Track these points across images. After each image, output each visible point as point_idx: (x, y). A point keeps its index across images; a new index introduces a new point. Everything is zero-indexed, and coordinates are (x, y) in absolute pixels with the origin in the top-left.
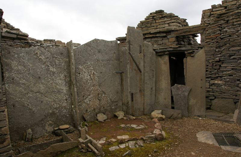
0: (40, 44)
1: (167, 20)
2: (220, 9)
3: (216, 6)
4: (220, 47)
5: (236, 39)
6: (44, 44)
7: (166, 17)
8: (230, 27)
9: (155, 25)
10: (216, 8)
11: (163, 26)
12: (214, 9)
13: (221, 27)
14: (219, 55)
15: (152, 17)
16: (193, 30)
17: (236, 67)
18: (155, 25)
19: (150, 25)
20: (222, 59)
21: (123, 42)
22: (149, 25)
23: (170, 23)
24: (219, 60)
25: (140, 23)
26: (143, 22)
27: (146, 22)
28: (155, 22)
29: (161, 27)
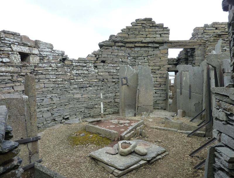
1: (159, 30)
3: (209, 25)
6: (6, 39)
7: (158, 27)
9: (144, 33)
10: (209, 27)
11: (154, 36)
12: (206, 28)
15: (141, 24)
16: (189, 45)
18: (144, 33)
19: (138, 33)
21: (107, 49)
22: (137, 32)
23: (162, 34)
25: (125, 28)
26: (130, 27)
27: (134, 28)
28: (144, 30)
29: (151, 37)
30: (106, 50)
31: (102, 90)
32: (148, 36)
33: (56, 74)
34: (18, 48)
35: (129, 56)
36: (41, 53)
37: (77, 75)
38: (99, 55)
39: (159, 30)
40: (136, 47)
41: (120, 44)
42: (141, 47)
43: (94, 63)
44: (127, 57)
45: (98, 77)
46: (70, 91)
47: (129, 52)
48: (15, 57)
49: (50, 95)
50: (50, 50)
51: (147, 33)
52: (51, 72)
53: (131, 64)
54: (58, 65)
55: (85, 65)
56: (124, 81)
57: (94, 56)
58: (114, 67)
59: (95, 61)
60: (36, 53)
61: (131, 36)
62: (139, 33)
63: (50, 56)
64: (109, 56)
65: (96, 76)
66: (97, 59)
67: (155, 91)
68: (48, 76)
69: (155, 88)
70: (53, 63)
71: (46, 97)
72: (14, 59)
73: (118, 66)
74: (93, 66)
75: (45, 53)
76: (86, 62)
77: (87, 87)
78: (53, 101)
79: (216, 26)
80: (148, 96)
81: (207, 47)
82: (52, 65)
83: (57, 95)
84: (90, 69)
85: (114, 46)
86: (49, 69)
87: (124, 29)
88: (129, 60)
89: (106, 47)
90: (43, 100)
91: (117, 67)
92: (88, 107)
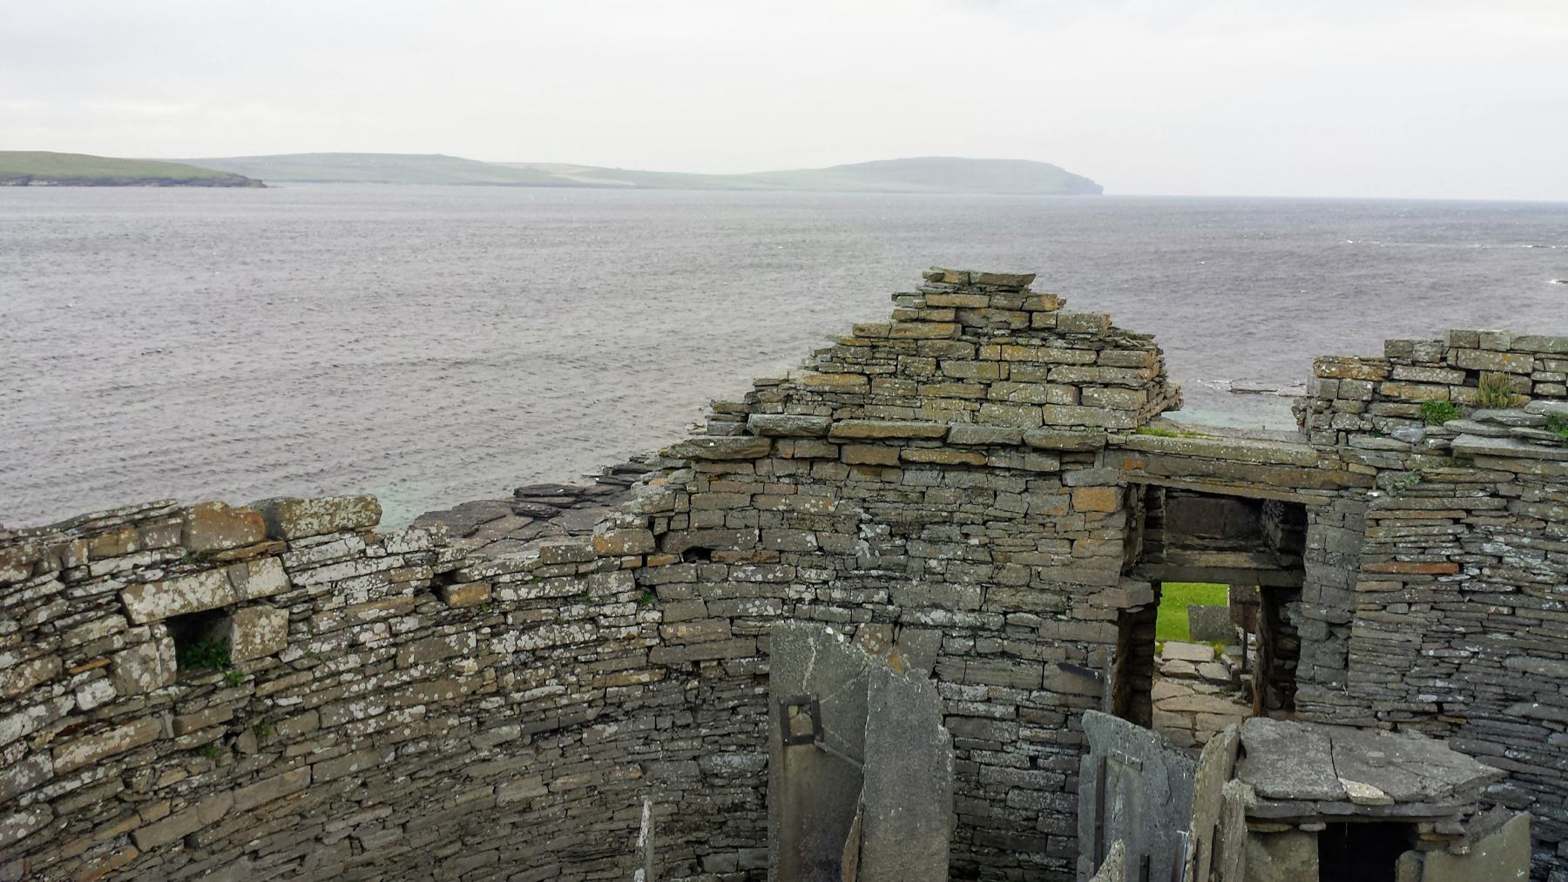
0: (61, 578)
1: (1069, 356)
2: (1440, 376)
4: (1450, 639)
5: (1552, 616)
7: (1062, 336)
8: (1526, 541)
10: (1414, 364)
13: (1470, 527)
14: (1439, 684)
17: (1538, 770)
18: (971, 370)
19: (930, 369)
20: (1457, 707)
21: (720, 476)
23: (1091, 383)
24: (1434, 708)
30: (716, 485)
31: (683, 734)
32: (993, 395)
33: (387, 689)
34: (165, 600)
35: (865, 516)
36: (299, 580)
37: (522, 657)
38: (670, 519)
39: (1069, 356)
40: (904, 464)
41: (806, 448)
42: (945, 468)
43: (634, 570)
44: (851, 526)
45: (660, 656)
46: (473, 771)
47: (866, 495)
48: (145, 661)
49: (341, 825)
50: (354, 543)
51: (990, 373)
52: (358, 682)
53: (879, 568)
54: (403, 628)
55: (578, 587)
56: (801, 722)
57: (637, 522)
58: (768, 587)
59: (644, 556)
60: (268, 589)
61: (886, 388)
62: (938, 367)
63: (350, 583)
64: (735, 520)
65: (650, 648)
66: (660, 539)
67: (1031, 750)
68: (335, 717)
69: (1027, 733)
70: (374, 621)
71: (318, 839)
72: (136, 675)
73: (792, 576)
74: (630, 584)
75: (325, 575)
76: (582, 569)
77: (585, 725)
78: (363, 849)
79: (1468, 359)
80: (918, 858)
81: (1377, 521)
82: (363, 638)
83: (384, 812)
84: (607, 610)
85: (768, 456)
86: (342, 668)
87: (844, 344)
88: (866, 545)
89: (719, 468)
90: (302, 858)
91: (786, 583)
92: (585, 848)
